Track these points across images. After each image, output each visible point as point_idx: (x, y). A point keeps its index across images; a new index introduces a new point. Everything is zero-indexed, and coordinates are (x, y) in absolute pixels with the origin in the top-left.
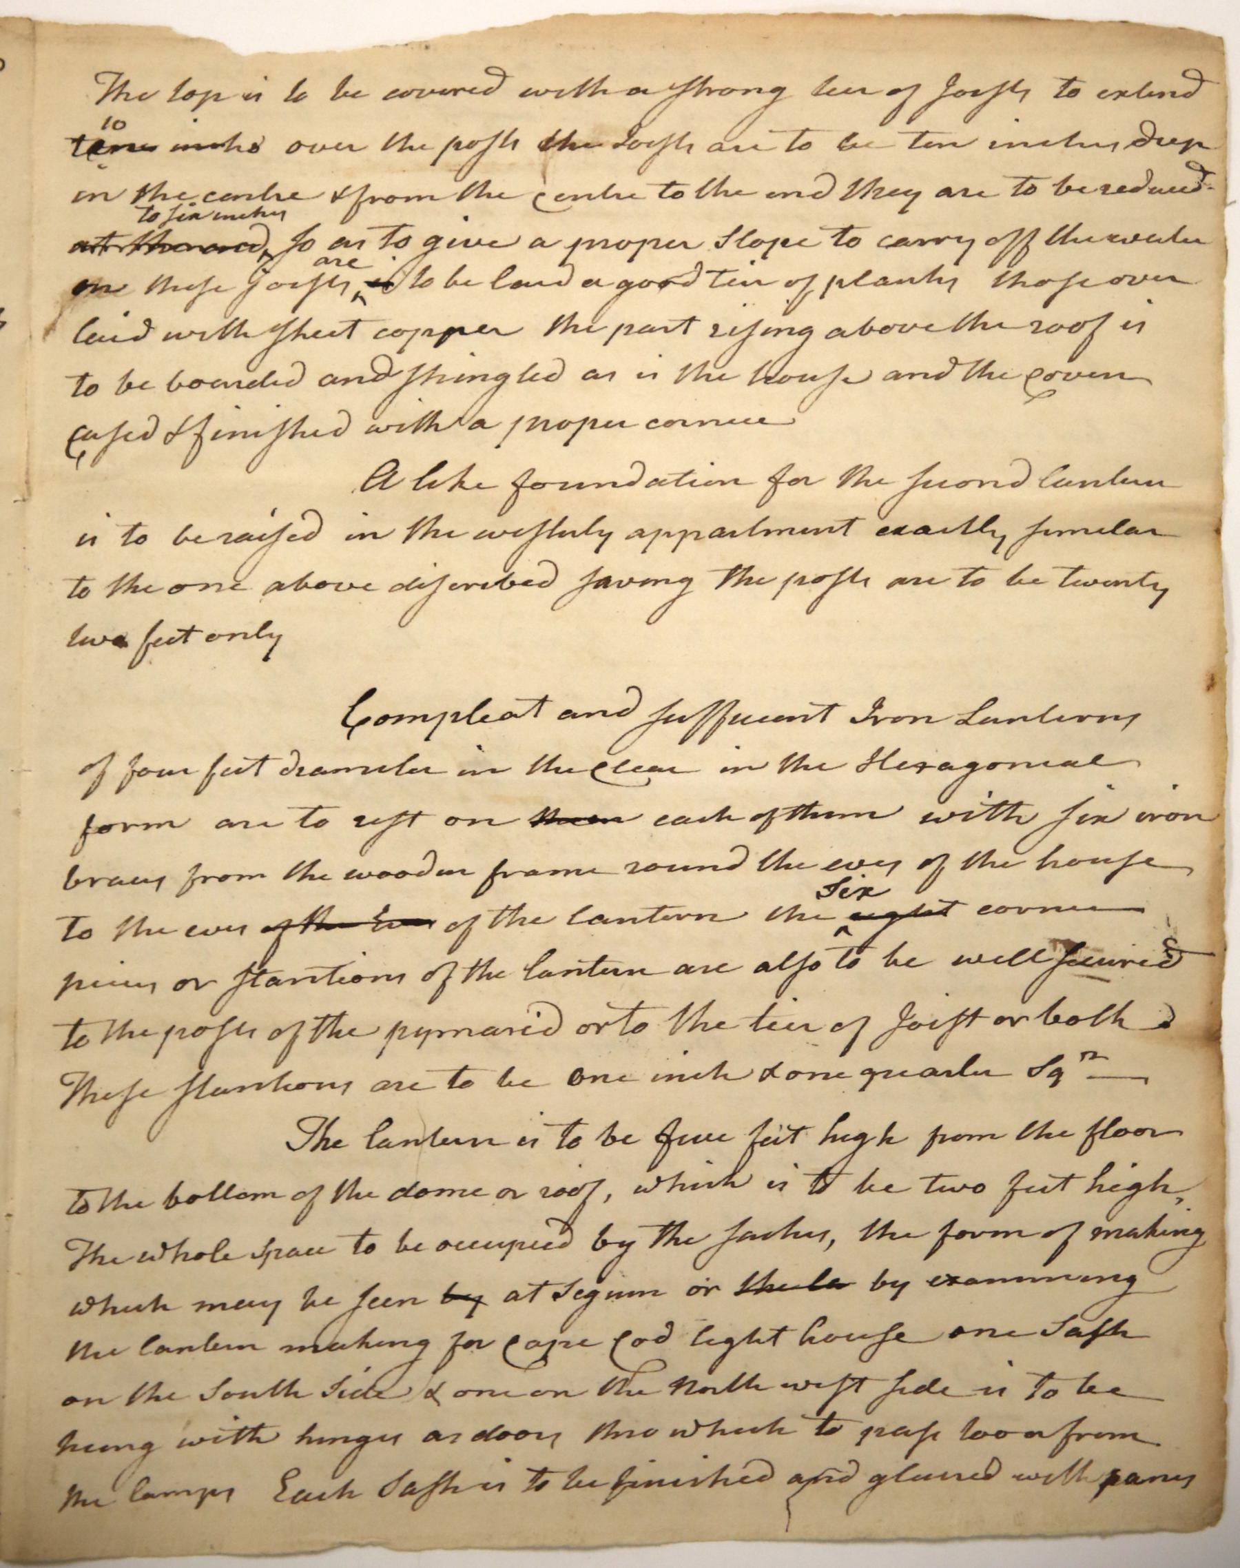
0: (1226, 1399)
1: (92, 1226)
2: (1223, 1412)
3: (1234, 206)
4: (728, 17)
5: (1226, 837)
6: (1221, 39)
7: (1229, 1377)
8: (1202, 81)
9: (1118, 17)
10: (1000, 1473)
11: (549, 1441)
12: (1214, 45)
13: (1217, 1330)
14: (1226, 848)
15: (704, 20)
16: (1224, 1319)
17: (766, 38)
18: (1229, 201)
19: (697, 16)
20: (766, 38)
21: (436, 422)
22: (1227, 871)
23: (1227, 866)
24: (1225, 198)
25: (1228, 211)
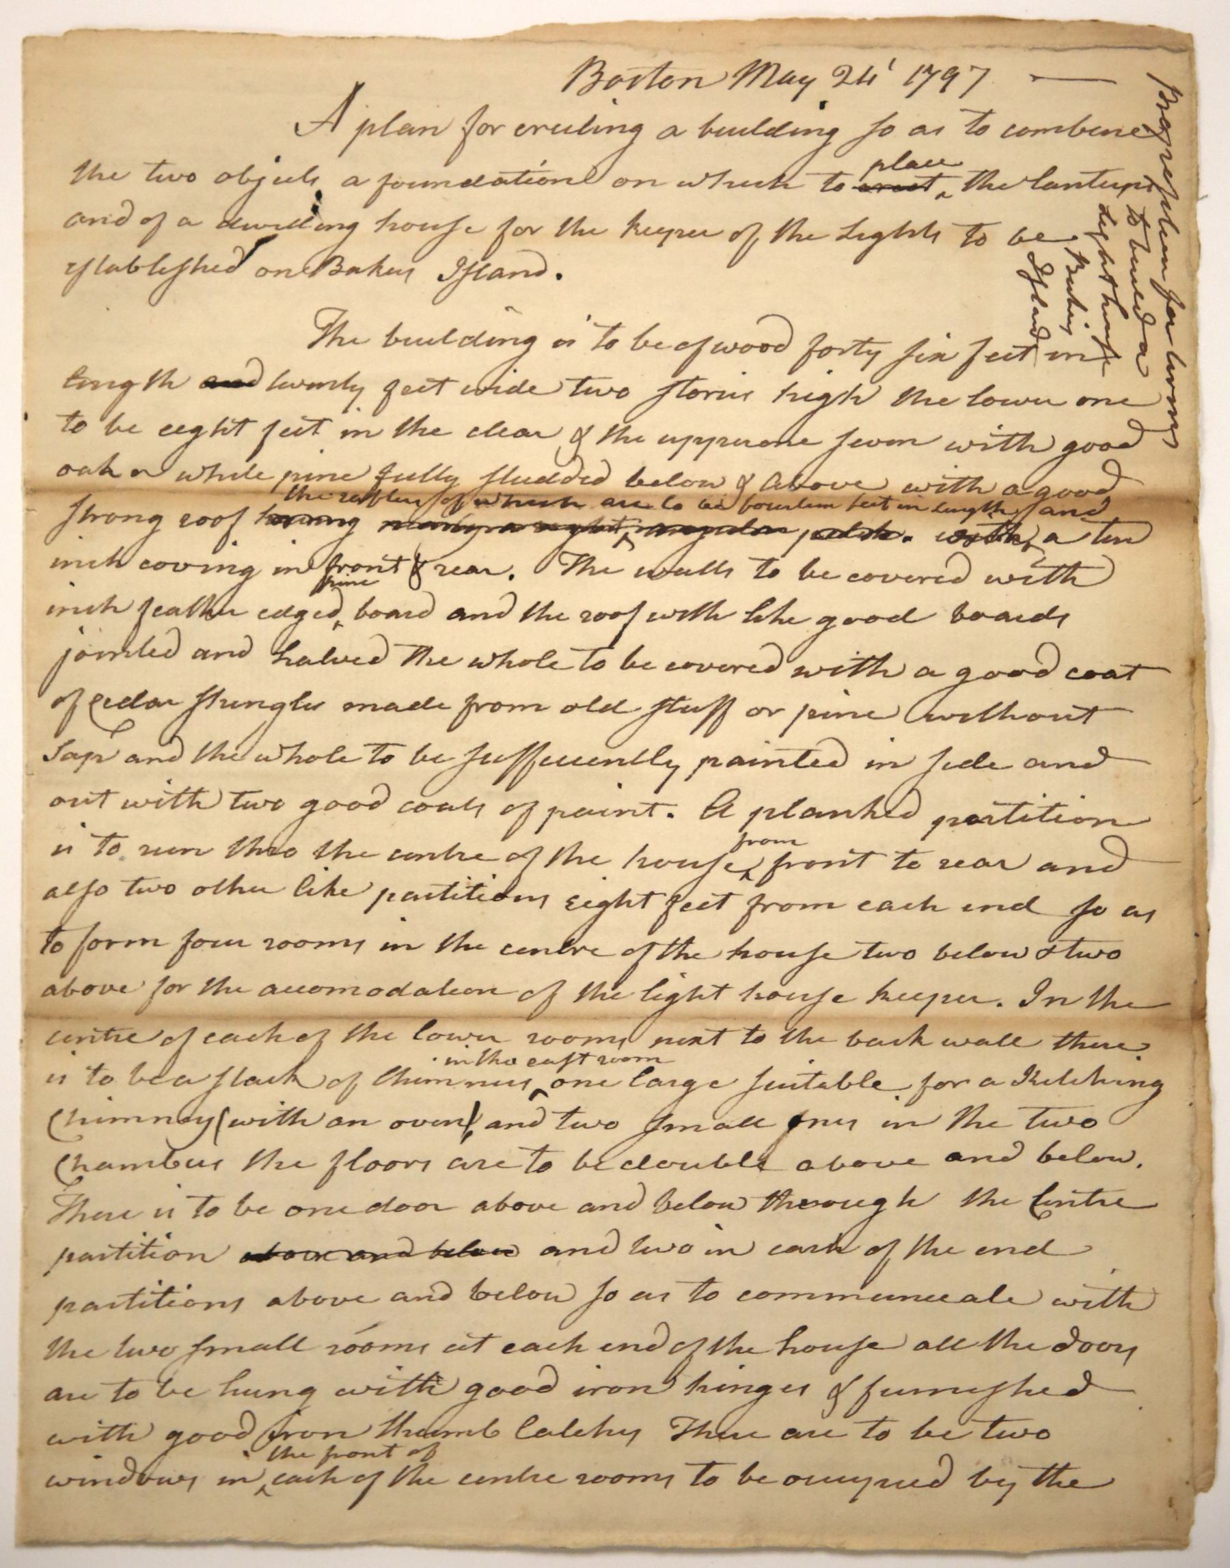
0: (1216, 1367)
1: (65, 1324)
2: (1214, 1382)
3: (1206, 200)
4: (704, 24)
5: (1208, 820)
6: (1190, 36)
7: (1219, 1344)
8: (1119, 476)
9: (1089, 15)
10: (54, 1165)
11: (664, 1482)
12: (1181, 45)
13: (1207, 1300)
14: (1208, 831)
15: (680, 27)
16: (1213, 1291)
17: (742, 44)
18: (1200, 196)
19: (674, 23)
20: (742, 44)
21: (340, 335)
22: (1209, 854)
23: (1209, 848)
24: (1197, 193)
25: (1200, 206)
